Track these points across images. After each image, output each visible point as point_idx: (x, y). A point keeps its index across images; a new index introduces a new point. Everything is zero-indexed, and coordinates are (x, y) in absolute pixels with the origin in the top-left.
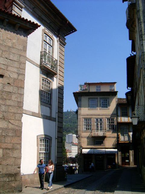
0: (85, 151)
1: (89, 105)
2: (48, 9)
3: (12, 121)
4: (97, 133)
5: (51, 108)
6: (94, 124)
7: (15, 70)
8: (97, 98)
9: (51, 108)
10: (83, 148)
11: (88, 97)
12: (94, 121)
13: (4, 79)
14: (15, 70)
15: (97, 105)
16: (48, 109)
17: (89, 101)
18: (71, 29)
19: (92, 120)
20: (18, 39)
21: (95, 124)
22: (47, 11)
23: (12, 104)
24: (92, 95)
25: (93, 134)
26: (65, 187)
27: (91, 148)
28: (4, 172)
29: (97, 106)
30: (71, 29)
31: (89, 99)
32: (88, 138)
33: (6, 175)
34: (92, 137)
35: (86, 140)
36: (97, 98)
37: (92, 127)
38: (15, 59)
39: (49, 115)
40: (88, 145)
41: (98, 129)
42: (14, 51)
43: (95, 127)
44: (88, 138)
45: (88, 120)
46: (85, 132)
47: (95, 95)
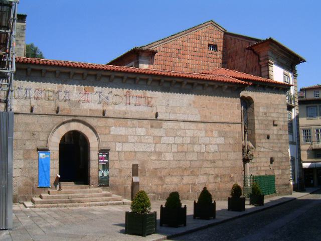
0: (306, 165)
1: (307, 114)
2: (285, 54)
3: (284, 152)
4: (317, 145)
5: (293, 135)
6: (314, 135)
7: (282, 119)
8: (316, 106)
9: (293, 135)
10: (303, 162)
11: (306, 105)
12: (314, 132)
13: (278, 126)
14: (282, 119)
15: (317, 114)
16: (291, 136)
17: (307, 110)
18: (298, 60)
19: (312, 131)
20: (281, 98)
21: (316, 135)
22: (285, 56)
23: (283, 142)
24: (310, 103)
25: (313, 147)
26: (310, 194)
27: (312, 162)
28: (283, 183)
29: (317, 116)
30: (298, 60)
31: (307, 107)
32: (308, 151)
33: (284, 184)
34: (313, 150)
35: (306, 153)
36: (316, 106)
37: (313, 139)
38: (282, 112)
39: (292, 141)
40: (308, 158)
41: (319, 141)
42: (280, 107)
43: (316, 139)
44: (308, 151)
45: (307, 132)
46: (304, 144)
47: (313, 103)
